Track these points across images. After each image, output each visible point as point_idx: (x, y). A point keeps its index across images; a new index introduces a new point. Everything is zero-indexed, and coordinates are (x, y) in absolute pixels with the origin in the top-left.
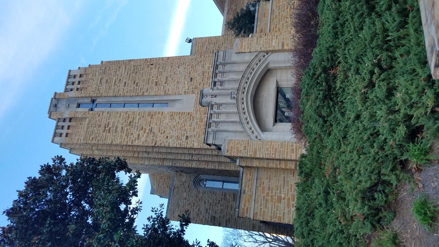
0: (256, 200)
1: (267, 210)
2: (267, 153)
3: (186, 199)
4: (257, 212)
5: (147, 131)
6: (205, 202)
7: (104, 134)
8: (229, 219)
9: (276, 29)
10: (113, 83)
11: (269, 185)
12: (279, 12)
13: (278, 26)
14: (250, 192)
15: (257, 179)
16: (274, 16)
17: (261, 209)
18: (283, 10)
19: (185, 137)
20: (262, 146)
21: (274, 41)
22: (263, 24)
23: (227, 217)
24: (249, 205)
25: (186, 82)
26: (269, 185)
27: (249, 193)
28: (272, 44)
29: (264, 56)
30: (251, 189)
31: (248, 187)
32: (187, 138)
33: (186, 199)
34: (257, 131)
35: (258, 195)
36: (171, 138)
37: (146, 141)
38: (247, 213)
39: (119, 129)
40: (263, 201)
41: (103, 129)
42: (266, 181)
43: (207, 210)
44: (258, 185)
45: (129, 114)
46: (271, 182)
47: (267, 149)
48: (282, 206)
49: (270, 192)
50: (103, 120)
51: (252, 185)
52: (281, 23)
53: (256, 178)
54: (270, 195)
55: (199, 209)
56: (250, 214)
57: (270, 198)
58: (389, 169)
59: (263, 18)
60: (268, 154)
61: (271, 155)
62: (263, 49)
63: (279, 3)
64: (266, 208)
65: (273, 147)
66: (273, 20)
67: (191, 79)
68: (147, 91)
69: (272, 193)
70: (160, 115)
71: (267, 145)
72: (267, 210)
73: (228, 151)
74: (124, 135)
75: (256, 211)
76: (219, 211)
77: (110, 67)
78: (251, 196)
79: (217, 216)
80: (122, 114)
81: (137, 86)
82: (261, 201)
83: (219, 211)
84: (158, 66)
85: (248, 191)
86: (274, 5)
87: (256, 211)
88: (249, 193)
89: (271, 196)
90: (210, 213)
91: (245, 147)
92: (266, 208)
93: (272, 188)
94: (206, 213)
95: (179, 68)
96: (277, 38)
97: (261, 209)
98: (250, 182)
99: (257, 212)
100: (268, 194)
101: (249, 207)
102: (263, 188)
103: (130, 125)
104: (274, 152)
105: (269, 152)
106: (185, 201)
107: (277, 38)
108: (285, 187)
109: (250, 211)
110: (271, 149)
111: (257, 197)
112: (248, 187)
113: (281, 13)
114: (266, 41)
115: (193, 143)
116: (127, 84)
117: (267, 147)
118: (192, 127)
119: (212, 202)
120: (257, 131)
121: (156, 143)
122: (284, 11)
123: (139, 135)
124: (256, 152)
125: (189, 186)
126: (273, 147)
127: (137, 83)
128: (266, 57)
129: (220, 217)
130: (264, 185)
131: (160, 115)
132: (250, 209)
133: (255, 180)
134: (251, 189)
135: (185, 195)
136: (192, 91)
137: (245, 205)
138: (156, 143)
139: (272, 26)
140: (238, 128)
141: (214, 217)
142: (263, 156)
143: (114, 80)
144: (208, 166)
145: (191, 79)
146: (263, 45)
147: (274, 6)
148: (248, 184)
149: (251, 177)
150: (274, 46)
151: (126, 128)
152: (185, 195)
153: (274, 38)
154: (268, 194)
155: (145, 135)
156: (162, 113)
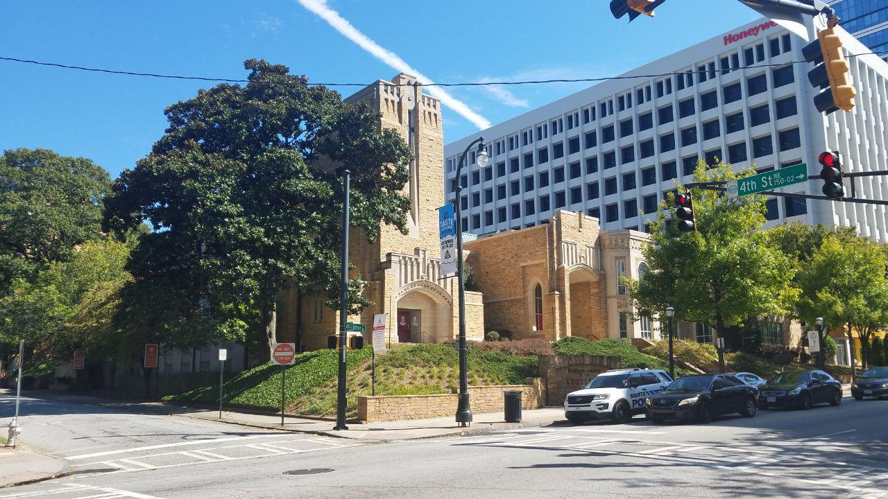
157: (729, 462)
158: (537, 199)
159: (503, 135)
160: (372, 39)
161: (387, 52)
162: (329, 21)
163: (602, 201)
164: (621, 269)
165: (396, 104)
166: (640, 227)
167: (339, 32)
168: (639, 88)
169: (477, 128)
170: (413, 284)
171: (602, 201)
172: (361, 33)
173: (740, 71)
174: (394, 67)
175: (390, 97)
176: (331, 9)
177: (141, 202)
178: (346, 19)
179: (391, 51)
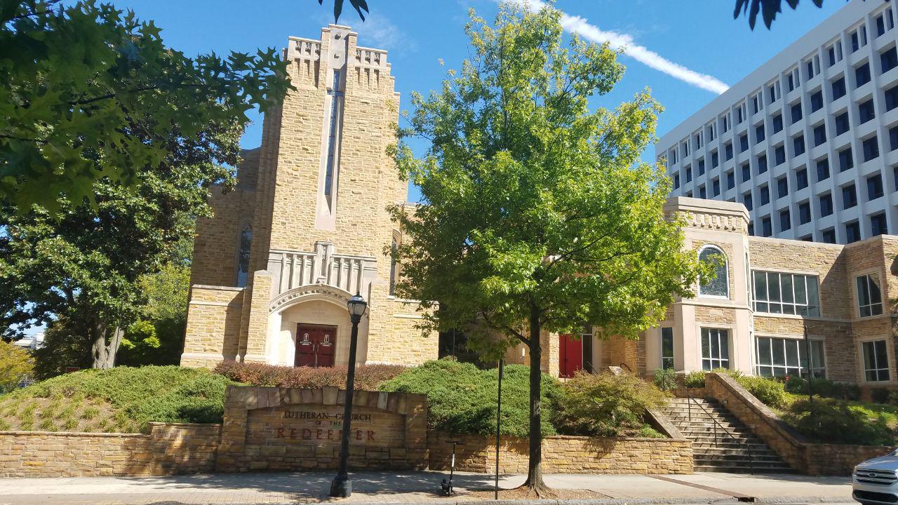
3: (226, 208)
5: (294, 173)
6: (223, 233)
7: (295, 115)
8: (202, 263)
10: (361, 121)
19: (284, 221)
21: (378, 325)
23: (205, 261)
25: (351, 218)
32: (284, 224)
33: (226, 208)
36: (284, 204)
37: (283, 172)
38: (196, 297)
39: (299, 135)
41: (301, 113)
43: (213, 235)
45: (317, 146)
48: (204, 333)
50: (313, 112)
55: (215, 225)
56: (195, 300)
67: (355, 225)
68: (345, 168)
70: (313, 188)
72: (750, 268)
73: (259, 277)
74: (292, 143)
76: (211, 250)
77: (382, 114)
79: (206, 249)
80: (319, 138)
81: (353, 154)
83: (211, 250)
84: (376, 180)
90: (209, 240)
91: (262, 296)
94: (210, 235)
95: (372, 208)
103: (304, 149)
106: (224, 206)
115: (277, 231)
116: (357, 140)
118: (296, 230)
119: (223, 241)
121: (278, 185)
123: (290, 162)
125: (243, 210)
127: (357, 155)
129: (205, 252)
131: (313, 188)
135: (231, 206)
136: (339, 227)
137: (204, 295)
138: (278, 185)
140: (295, 285)
141: (205, 245)
143: (364, 121)
144: (253, 246)
145: (355, 225)
151: (300, 144)
152: (231, 206)
155: (290, 171)
156: (316, 191)
157: (377, 447)
158: (853, 108)
159: (743, 96)
160: (684, 66)
161: (701, 76)
162: (636, 57)
163: (840, 217)
164: (727, 120)
165: (312, 64)
166: (814, 237)
167: (647, 66)
168: (876, 14)
169: (717, 94)
170: (302, 290)
171: (840, 217)
172: (671, 63)
173: (293, 426)
174: (710, 90)
175: (304, 55)
176: (637, 46)
177: (86, 328)
178: (654, 52)
179: (706, 73)
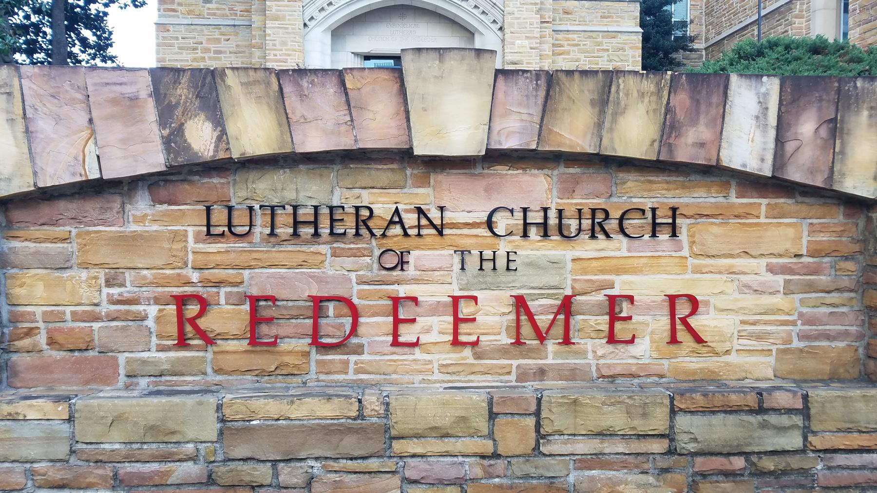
0: (193, 27)
1: (177, 50)
2: (277, 43)
4: (168, 30)
9: (568, 45)
11: (225, 52)
12: (608, 50)
13: (576, 48)
14: (208, 14)
15: (234, 26)
16: (600, 40)
17: (177, 38)
18: (611, 58)
20: (290, 30)
21: (526, 42)
22: (583, 15)
24: (182, 13)
26: (225, 52)
27: (206, 11)
28: (518, 38)
29: (494, 21)
30: (214, 14)
31: (218, 9)
34: (326, 18)
35: (202, 30)
40: (191, 41)
42: (231, 45)
44: (223, 29)
46: (232, 55)
47: (284, 43)
49: (212, 55)
51: (223, 16)
52: (582, 56)
53: (237, 23)
54: (206, 55)
57: (200, 55)
58: (805, 310)
59: (599, 15)
60: (274, 45)
61: (273, 52)
62: (508, 19)
63: (631, 48)
64: (180, 48)
65: (289, 55)
66: (590, 37)
69: (210, 58)
71: (293, 41)
72: (177, 50)
75: (171, 28)
78: (199, 16)
82: (191, 38)
85: (209, 9)
86: (627, 38)
87: (171, 28)
88: (206, 11)
89: (204, 58)
92: (180, 48)
93: (219, 59)
96: (531, 48)
97: (177, 38)
98: (228, 12)
99: (168, 30)
100: (207, 50)
101: (179, 14)
102: (218, 41)
104: (278, 57)
105: (278, 47)
107: (531, 48)
108: (605, 47)
109: (170, 16)
110: (284, 52)
111: (199, 28)
112: (218, 9)
113: (606, 54)
114: (528, 26)
117: (289, 43)
120: (326, 18)
122: (611, 61)
124: (276, 18)
126: (289, 55)
128: (492, 26)
130: (223, 42)
132: (174, 16)
133: (232, 23)
134: (214, 14)
139: (575, 36)
142: (269, 35)
146: (519, 18)
147: (624, 37)
148: (224, 7)
149: (238, 13)
150: (513, 44)
153: (534, 41)
154: (207, 50)
